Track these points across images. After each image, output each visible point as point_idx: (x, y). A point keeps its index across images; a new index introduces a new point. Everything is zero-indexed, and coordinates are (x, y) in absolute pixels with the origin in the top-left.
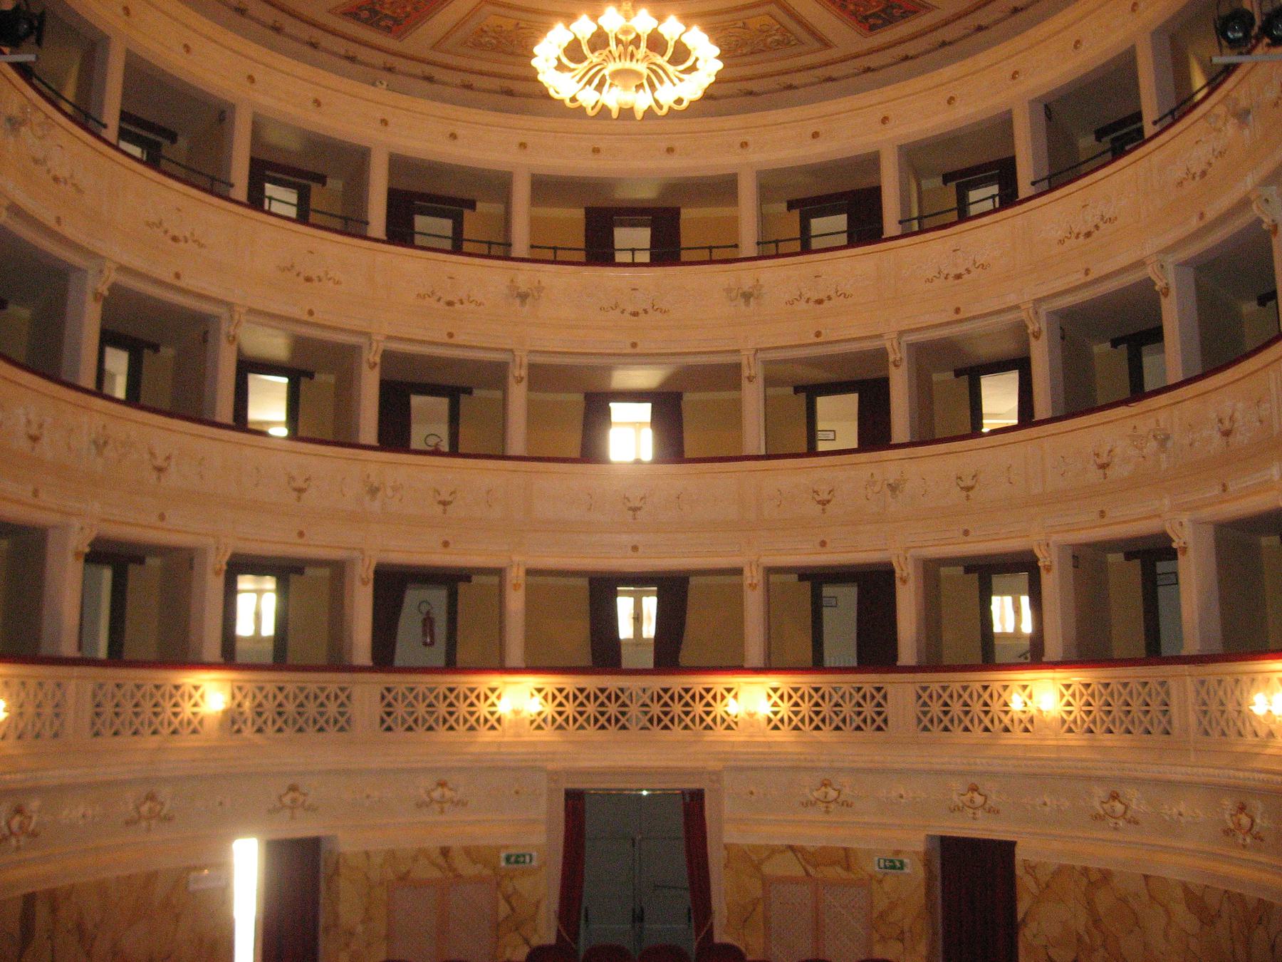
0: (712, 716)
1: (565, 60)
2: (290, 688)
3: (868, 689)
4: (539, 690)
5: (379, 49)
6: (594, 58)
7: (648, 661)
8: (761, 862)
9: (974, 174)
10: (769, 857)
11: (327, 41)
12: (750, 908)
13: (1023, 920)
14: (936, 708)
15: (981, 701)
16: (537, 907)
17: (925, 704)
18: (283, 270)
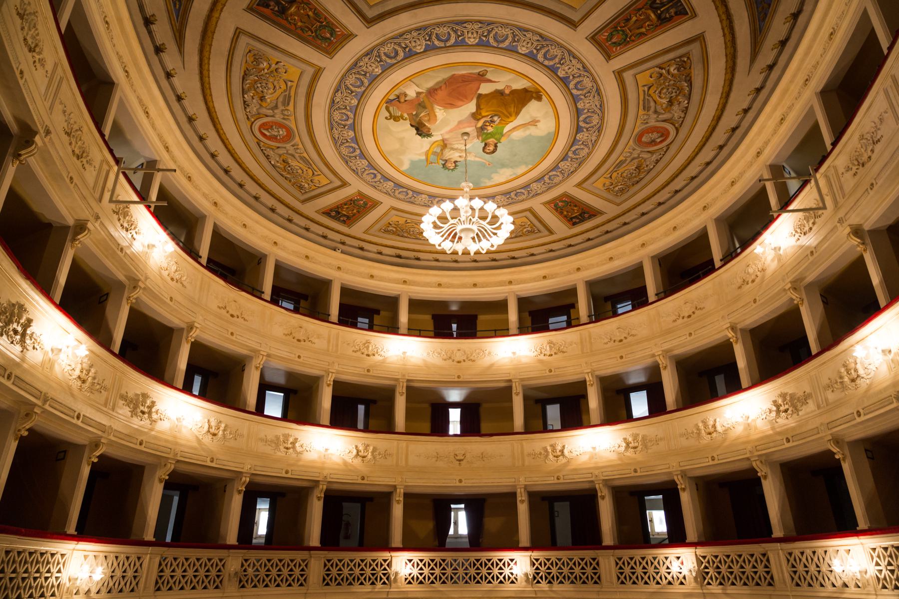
1: (438, 223)
2: (252, 560)
3: (576, 559)
5: (338, 232)
6: (452, 221)
7: (466, 543)
9: (617, 295)
11: (314, 227)
15: (665, 566)
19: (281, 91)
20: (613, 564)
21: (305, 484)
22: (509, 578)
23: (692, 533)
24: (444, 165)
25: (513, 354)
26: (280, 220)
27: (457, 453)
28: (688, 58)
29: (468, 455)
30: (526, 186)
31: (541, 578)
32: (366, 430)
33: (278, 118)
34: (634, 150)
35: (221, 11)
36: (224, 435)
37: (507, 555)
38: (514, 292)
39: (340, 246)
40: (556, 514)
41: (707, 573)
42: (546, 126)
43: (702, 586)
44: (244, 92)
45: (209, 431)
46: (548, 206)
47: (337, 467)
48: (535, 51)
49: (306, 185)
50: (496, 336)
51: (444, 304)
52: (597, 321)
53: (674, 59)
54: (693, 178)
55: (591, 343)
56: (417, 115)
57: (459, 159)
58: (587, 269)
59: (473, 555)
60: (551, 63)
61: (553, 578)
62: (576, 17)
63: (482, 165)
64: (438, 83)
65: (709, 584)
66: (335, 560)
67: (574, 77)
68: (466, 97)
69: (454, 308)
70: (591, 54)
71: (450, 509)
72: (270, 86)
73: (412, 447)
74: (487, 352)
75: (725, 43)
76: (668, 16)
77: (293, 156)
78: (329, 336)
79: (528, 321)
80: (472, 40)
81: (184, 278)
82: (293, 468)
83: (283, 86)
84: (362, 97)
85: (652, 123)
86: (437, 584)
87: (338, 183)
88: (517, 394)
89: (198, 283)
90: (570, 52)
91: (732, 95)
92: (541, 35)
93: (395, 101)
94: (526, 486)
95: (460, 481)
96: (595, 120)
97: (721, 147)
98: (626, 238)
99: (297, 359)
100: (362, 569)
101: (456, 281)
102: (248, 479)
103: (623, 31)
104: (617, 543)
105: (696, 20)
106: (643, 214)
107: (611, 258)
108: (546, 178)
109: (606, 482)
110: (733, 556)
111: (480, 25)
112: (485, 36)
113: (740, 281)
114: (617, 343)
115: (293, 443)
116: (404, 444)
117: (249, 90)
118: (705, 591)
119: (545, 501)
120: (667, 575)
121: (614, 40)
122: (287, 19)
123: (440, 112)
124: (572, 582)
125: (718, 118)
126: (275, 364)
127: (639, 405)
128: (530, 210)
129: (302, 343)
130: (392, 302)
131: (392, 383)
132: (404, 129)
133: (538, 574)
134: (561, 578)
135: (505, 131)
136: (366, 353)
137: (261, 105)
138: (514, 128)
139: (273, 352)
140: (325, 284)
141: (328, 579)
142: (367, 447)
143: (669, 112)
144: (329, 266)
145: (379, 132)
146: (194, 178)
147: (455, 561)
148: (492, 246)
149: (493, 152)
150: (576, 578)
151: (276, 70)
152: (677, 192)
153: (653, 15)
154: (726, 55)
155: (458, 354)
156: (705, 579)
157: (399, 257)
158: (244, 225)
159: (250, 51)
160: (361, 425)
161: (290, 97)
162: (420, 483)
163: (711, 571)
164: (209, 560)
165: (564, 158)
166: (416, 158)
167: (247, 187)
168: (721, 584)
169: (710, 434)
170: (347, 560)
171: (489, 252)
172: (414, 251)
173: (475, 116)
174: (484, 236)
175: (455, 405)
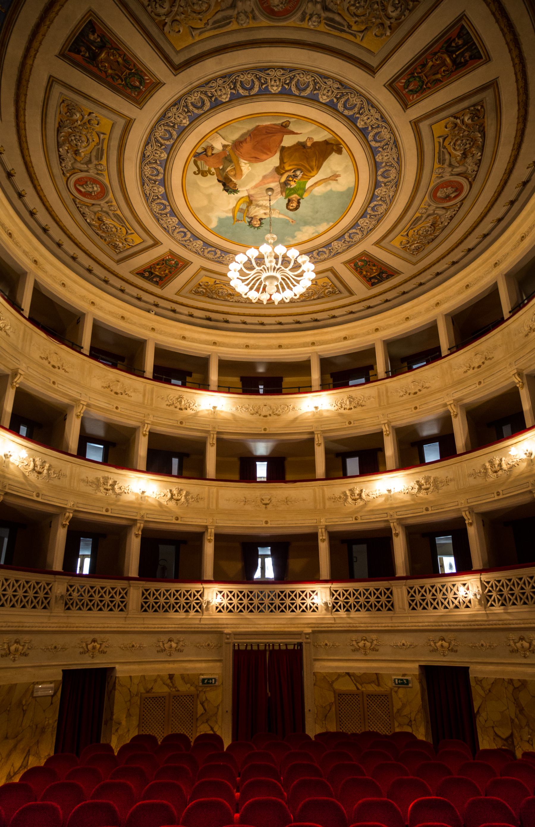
0: (305, 605)
3: (372, 589)
4: (221, 592)
5: (151, 294)
8: (333, 682)
9: (413, 352)
10: (337, 679)
12: (328, 708)
13: (478, 711)
14: (418, 597)
16: (218, 709)
17: (412, 596)
18: (105, 388)
19: (94, 144)
20: (405, 592)
21: (124, 522)
22: (311, 607)
23: (477, 563)
24: (250, 222)
25: (316, 406)
26: (97, 281)
27: (263, 497)
28: (482, 107)
29: (274, 500)
30: (328, 245)
31: (340, 607)
32: (180, 476)
33: (92, 173)
34: (429, 206)
35: (35, 57)
36: (48, 474)
37: (308, 587)
38: (317, 353)
39: (154, 308)
40: (355, 560)
41: (491, 596)
42: (346, 182)
43: (485, 608)
44: (59, 145)
45: (34, 469)
46: (348, 265)
47: (153, 508)
48: (335, 100)
49: (121, 245)
50: (300, 393)
51: (251, 365)
52: (393, 376)
53: (468, 108)
54: (485, 236)
55: (388, 397)
56: (224, 170)
57: (264, 217)
58: (384, 329)
59: (279, 587)
60: (351, 113)
61: (350, 606)
62: (374, 62)
63: (286, 222)
64: (242, 136)
65: (492, 605)
66: (153, 590)
67: (372, 128)
68: (269, 150)
69: (261, 370)
70: (387, 102)
71: (257, 556)
72: (84, 138)
73: (222, 492)
74: (291, 407)
75: (518, 90)
76: (463, 60)
77: (107, 213)
78: (145, 390)
79: (331, 381)
80: (275, 88)
81: (8, 327)
82: (112, 507)
83: (96, 139)
84: (171, 150)
85: (447, 177)
86: (245, 613)
87: (151, 242)
88: (319, 445)
89: (21, 333)
90: (369, 101)
91: (524, 146)
92: (341, 83)
93: (202, 154)
94: (326, 526)
95: (266, 522)
96: (393, 174)
97: (512, 203)
98: (422, 298)
99: (115, 410)
100: (177, 599)
101: (262, 343)
102: (71, 515)
103: (420, 77)
104: (409, 575)
105: (489, 64)
106: (438, 274)
107: (407, 318)
108: (346, 236)
109: (400, 521)
110: (515, 580)
111: (282, 72)
112: (288, 84)
113: (527, 329)
114: (412, 395)
115: (113, 485)
116: (214, 490)
117: (64, 144)
118: (488, 612)
119: (345, 543)
120: (454, 600)
121: (411, 87)
122: (97, 66)
123: (245, 167)
124: (368, 610)
125: (509, 172)
126: (95, 414)
127: (432, 453)
128: (332, 270)
129: (120, 395)
130: (202, 363)
131: (203, 435)
132: (211, 185)
133: (337, 603)
134: (357, 606)
135: (308, 185)
136: (179, 407)
137: (75, 160)
138: (316, 183)
139: (92, 402)
140: (141, 344)
141: (146, 606)
142: (180, 491)
143: (463, 165)
144: (143, 326)
145: (188, 188)
146: (15, 235)
147: (262, 592)
148: (295, 295)
149: (296, 209)
150: (371, 606)
151: (89, 121)
152: (470, 250)
153: (448, 60)
154: (519, 103)
155: (265, 409)
156: (488, 601)
157: (209, 319)
158: (63, 284)
159: (63, 101)
160: (175, 471)
161: (102, 150)
162: (230, 524)
163: (494, 594)
164: (38, 583)
165: (363, 215)
166: (223, 215)
167: (64, 246)
168: (503, 605)
169: (496, 472)
170: (163, 590)
171: (292, 301)
172: (223, 313)
173: (279, 171)
174: (289, 287)
175: (262, 459)
